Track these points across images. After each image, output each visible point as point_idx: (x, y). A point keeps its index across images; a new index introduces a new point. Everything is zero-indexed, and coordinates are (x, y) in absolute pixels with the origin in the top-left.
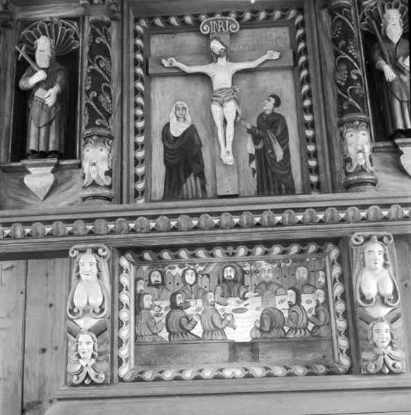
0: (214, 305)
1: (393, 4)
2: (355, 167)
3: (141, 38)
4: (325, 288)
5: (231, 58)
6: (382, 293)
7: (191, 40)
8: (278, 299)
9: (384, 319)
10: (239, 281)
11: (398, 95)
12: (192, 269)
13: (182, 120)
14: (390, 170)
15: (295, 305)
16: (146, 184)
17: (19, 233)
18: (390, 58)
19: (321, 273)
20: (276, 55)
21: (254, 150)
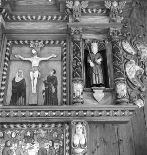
0: (21, 146)
1: (96, 41)
2: (76, 96)
3: (9, 47)
4: (63, 141)
5: (39, 56)
6: (81, 143)
7: (27, 49)
8: (46, 144)
9: (80, 153)
10: (32, 137)
11: (94, 72)
12: (15, 132)
13: (20, 77)
14: (90, 98)
15: (51, 147)
16: (4, 99)
17: (126, 114)
18: (93, 60)
19: (62, 135)
20: (55, 56)
21: (45, 89)
